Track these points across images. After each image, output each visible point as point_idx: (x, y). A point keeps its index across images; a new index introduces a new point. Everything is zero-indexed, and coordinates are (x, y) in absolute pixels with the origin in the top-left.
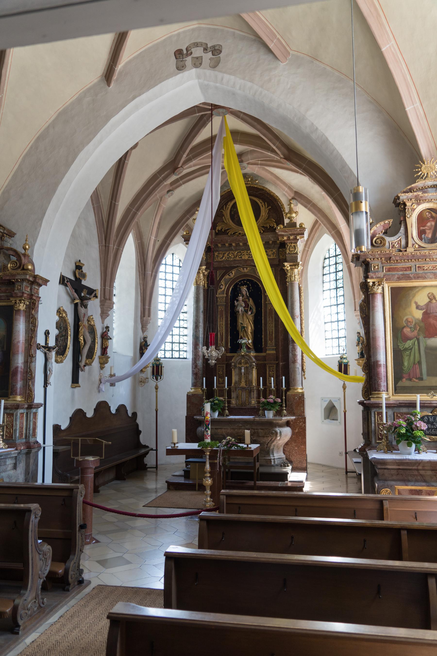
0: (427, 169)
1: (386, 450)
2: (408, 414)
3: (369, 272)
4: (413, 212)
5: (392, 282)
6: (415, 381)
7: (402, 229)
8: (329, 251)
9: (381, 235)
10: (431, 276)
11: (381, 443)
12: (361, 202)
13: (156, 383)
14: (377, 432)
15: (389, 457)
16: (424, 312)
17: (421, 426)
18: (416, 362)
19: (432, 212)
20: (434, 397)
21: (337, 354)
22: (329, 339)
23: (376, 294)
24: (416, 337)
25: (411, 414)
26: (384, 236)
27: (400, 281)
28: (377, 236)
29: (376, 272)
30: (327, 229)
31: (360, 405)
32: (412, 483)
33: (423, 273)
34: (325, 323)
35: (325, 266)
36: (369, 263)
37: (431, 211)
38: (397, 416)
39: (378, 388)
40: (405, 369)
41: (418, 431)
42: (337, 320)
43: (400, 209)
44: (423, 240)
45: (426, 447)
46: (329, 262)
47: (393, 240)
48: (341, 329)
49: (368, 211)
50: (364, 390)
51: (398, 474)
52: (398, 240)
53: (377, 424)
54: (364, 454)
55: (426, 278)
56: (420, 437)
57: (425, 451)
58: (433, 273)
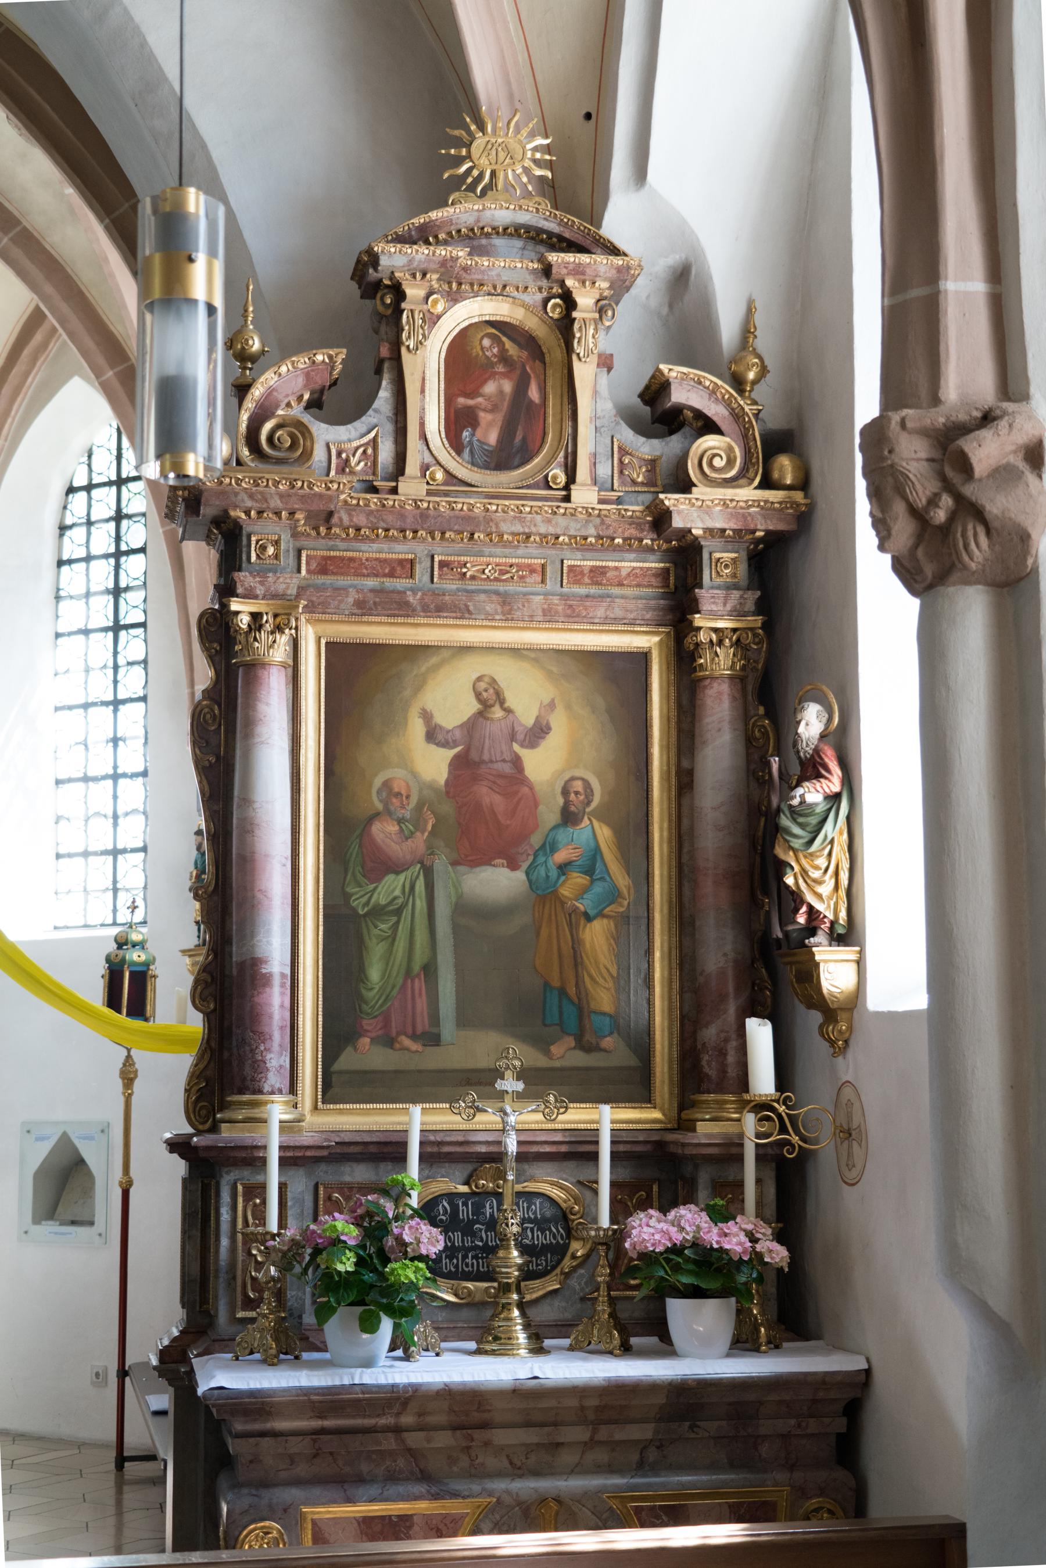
0: (494, 152)
1: (273, 1352)
2: (366, 1189)
3: (240, 570)
4: (431, 328)
5: (332, 621)
6: (408, 1049)
7: (385, 394)
8: (90, 457)
9: (297, 411)
10: (489, 608)
11: (253, 1320)
12: (191, 260)
14: (239, 1273)
15: (284, 1384)
16: (456, 757)
17: (419, 1242)
18: (417, 968)
19: (504, 339)
20: (480, 1117)
21: (102, 925)
22: (70, 855)
23: (264, 665)
24: (421, 862)
25: (385, 1192)
26: (307, 419)
27: (365, 619)
28: (280, 412)
29: (270, 570)
30: (85, 354)
31: (175, 1156)
32: (374, 1490)
33: (458, 590)
34: (58, 782)
35: (68, 522)
36: (241, 528)
37: (505, 334)
38: (329, 1198)
39: (253, 1080)
40: (371, 994)
41: (407, 1262)
42: (111, 772)
43: (380, 308)
44: (466, 452)
45: (437, 1329)
46: (90, 506)
47: (345, 437)
48: (127, 814)
49: (218, 302)
50: (196, 1088)
51: (315, 1456)
52: (365, 440)
53: (240, 1236)
54: (179, 1371)
55: (469, 612)
56: (412, 1286)
57: (433, 1349)
58: (497, 593)
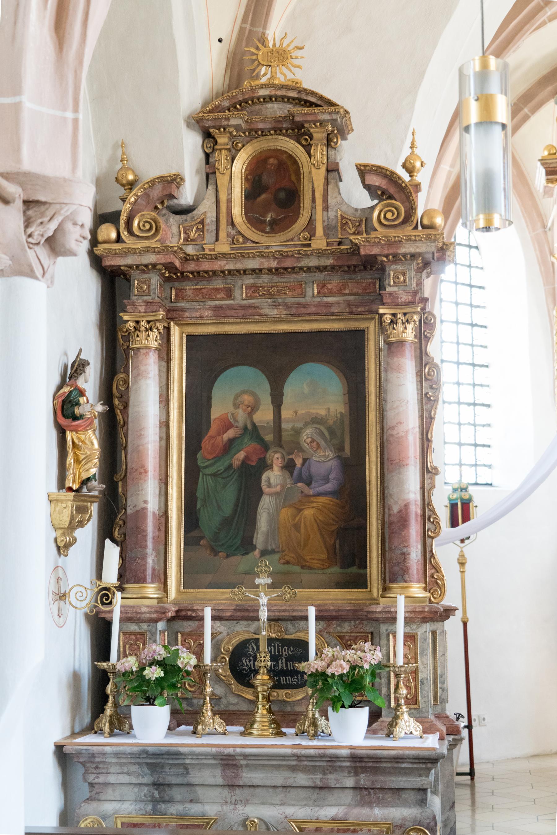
13: (459, 549)
